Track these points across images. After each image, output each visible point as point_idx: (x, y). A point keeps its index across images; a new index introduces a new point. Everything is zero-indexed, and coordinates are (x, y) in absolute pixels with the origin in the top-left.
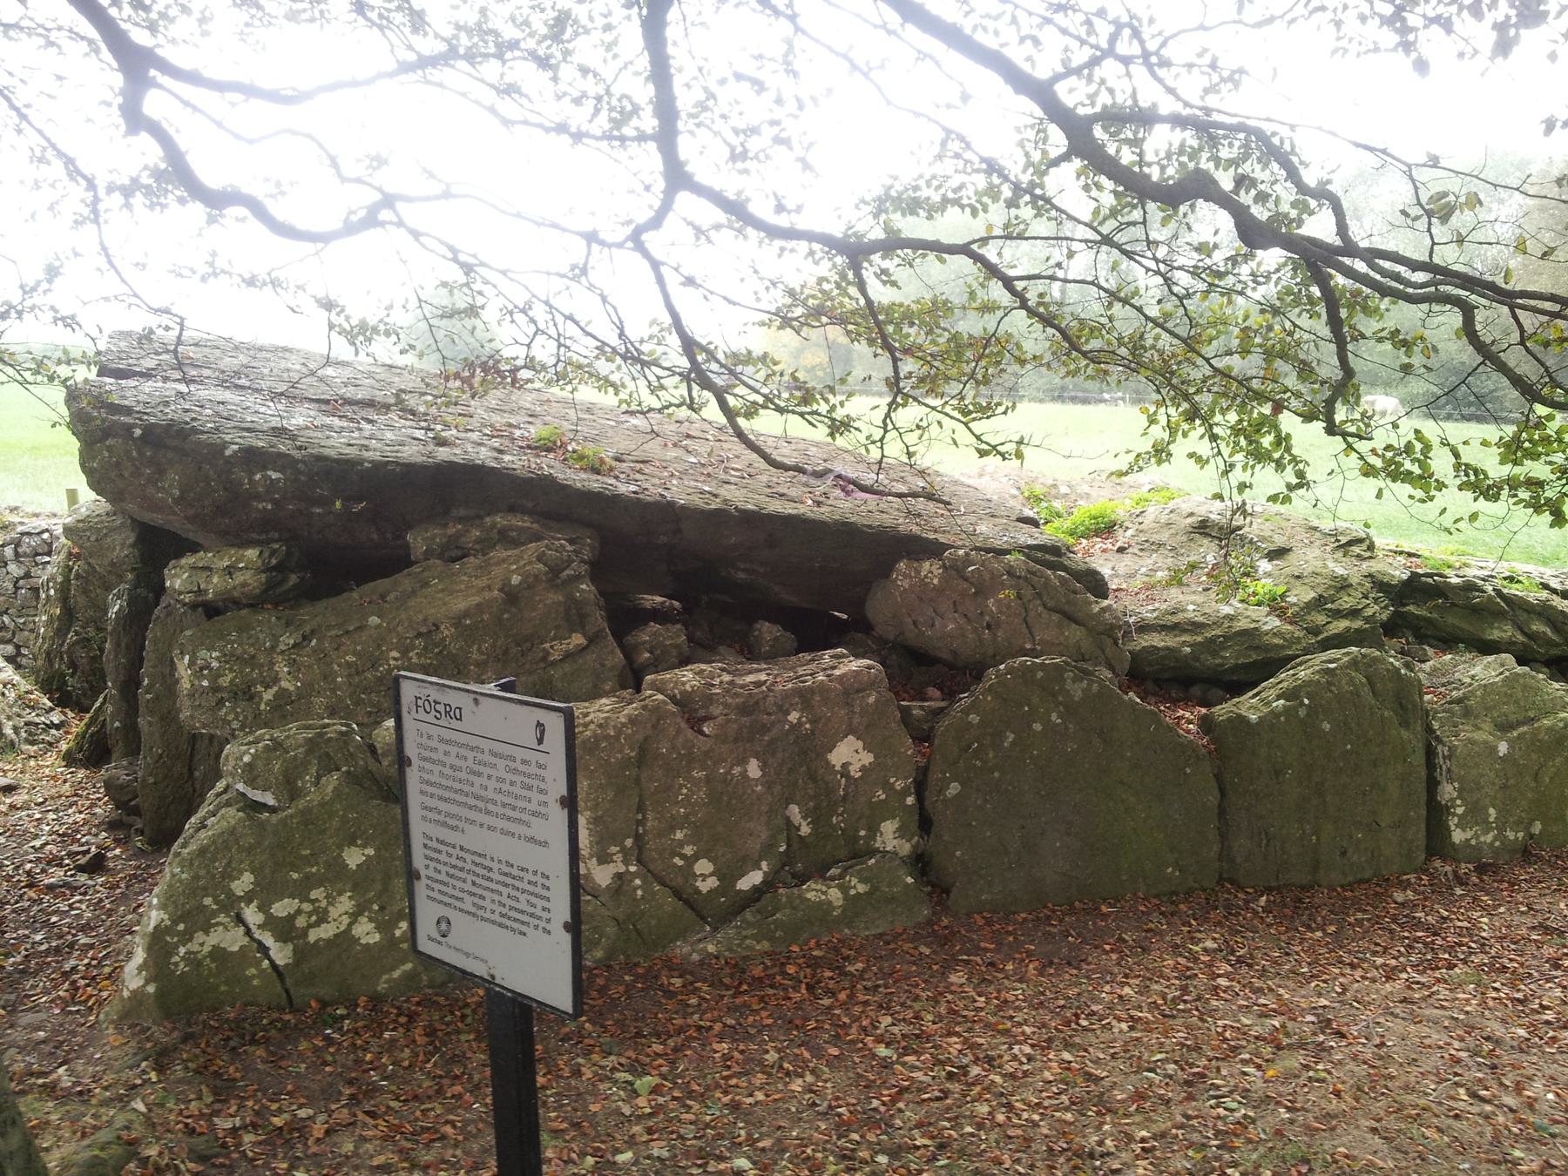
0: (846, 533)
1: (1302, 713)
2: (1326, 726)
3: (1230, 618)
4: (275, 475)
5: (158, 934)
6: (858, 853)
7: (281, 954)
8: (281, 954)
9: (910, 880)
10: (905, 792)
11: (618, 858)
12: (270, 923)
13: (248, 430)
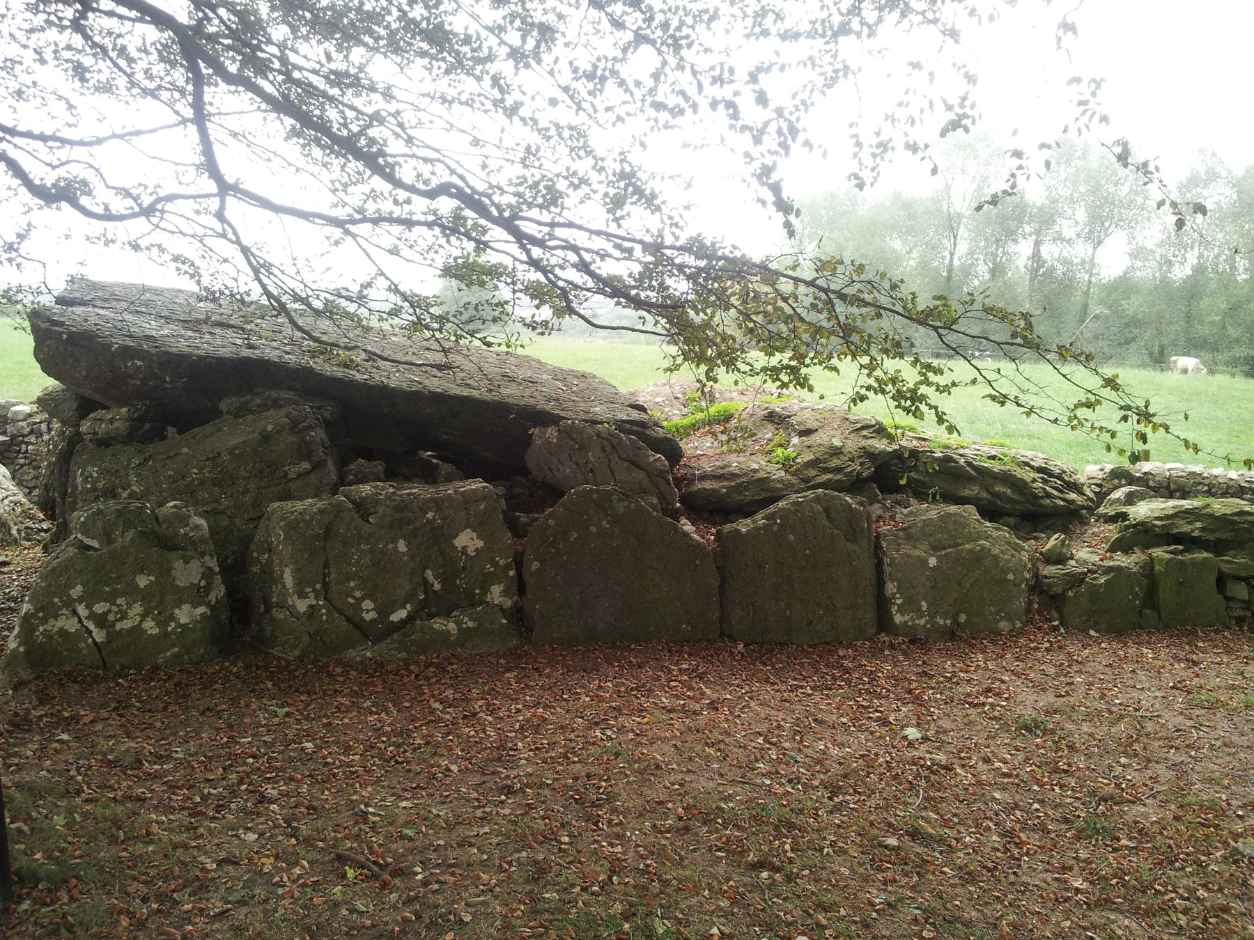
0: (501, 409)
1: (775, 528)
2: (792, 538)
3: (755, 471)
4: (139, 363)
5: (27, 618)
7: (99, 636)
8: (99, 636)
9: (504, 621)
11: (312, 595)
12: (92, 616)
13: (130, 336)
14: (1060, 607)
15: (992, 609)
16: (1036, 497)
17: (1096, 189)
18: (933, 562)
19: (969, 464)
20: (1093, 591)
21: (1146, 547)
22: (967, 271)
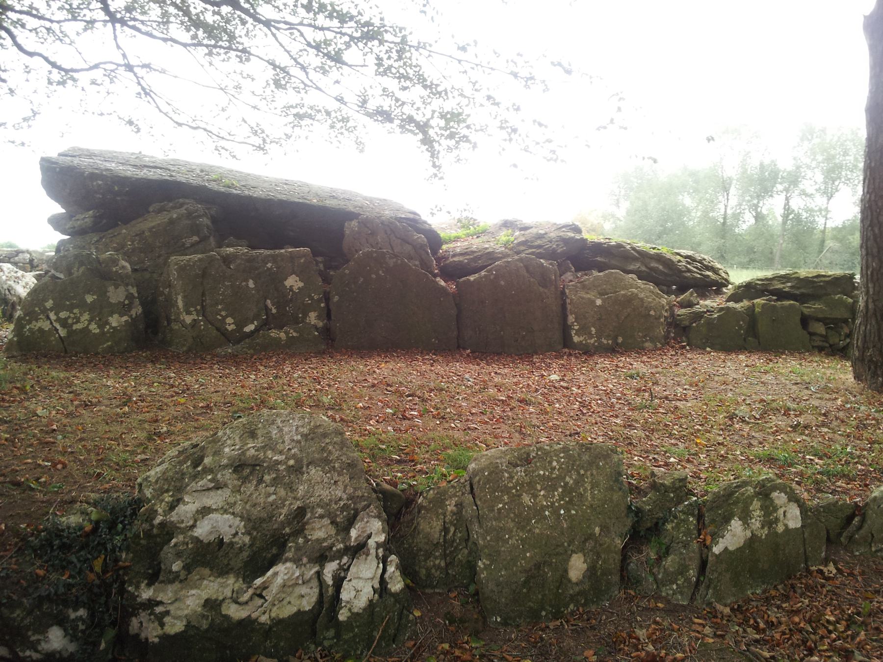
1: (492, 277)
3: (486, 248)
4: (100, 182)
6: (296, 321)
7: (63, 332)
8: (63, 332)
12: (58, 320)
14: (687, 334)
15: (640, 334)
16: (680, 271)
17: (830, 159)
18: (599, 302)
19: (634, 249)
20: (710, 323)
21: (751, 298)
22: (737, 217)
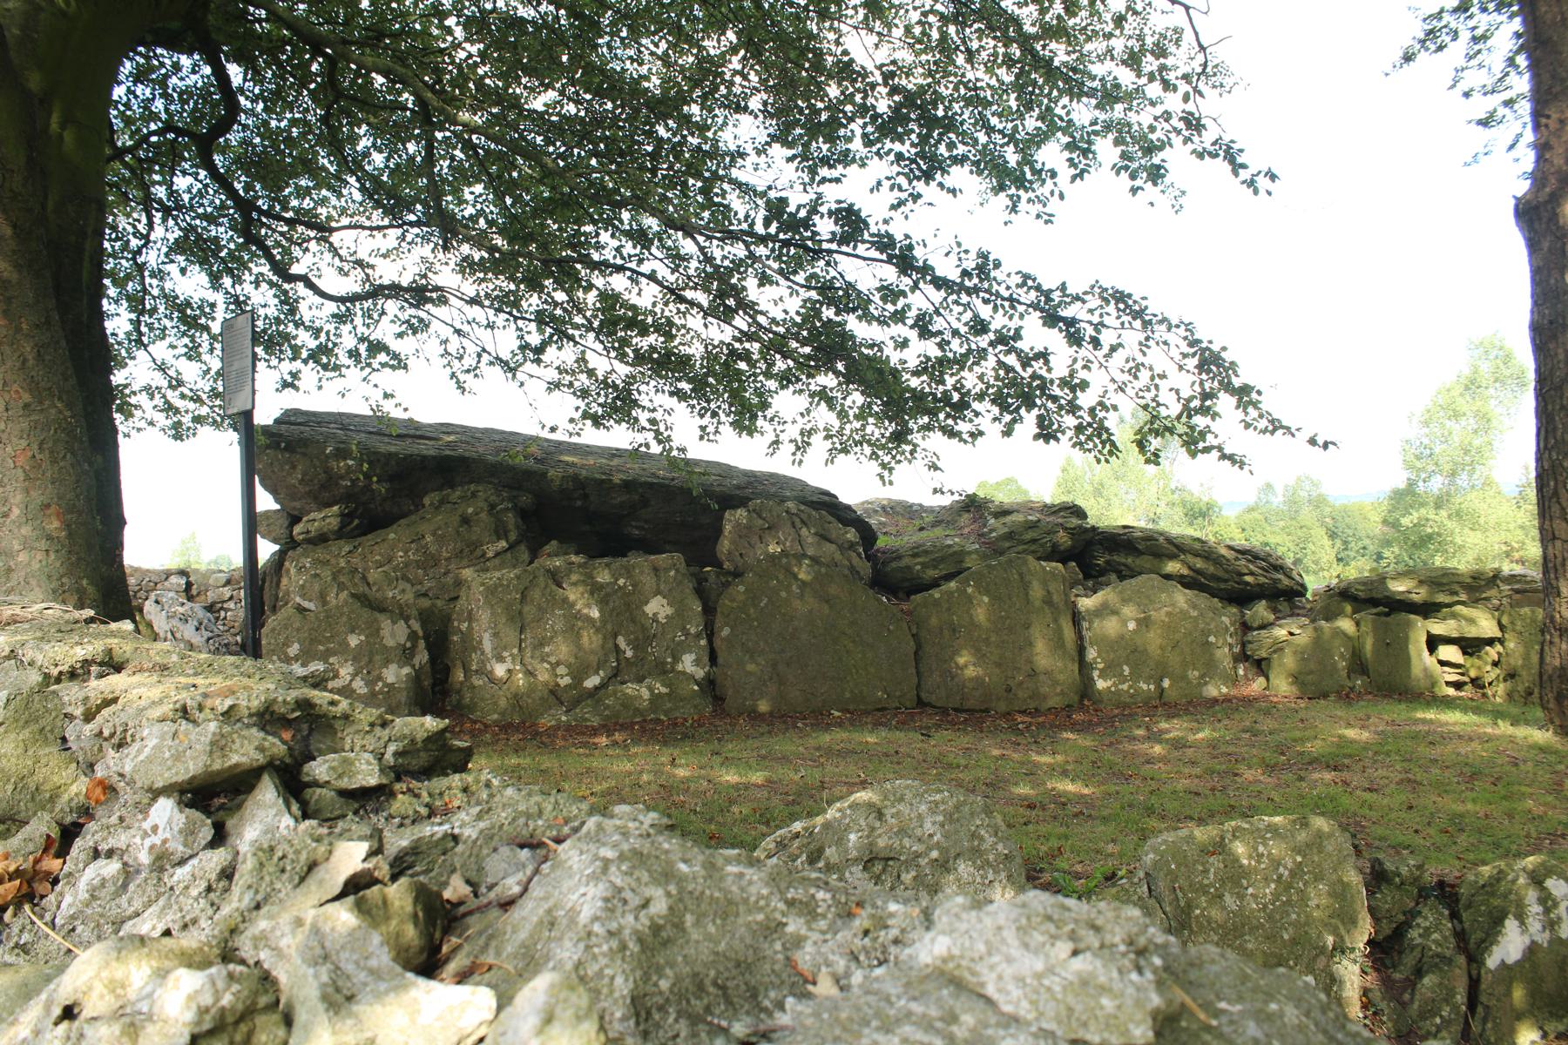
3: (950, 546)
4: (351, 462)
10: (698, 636)
